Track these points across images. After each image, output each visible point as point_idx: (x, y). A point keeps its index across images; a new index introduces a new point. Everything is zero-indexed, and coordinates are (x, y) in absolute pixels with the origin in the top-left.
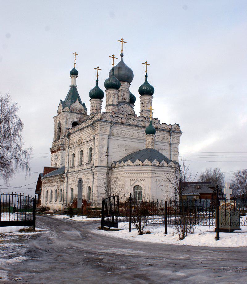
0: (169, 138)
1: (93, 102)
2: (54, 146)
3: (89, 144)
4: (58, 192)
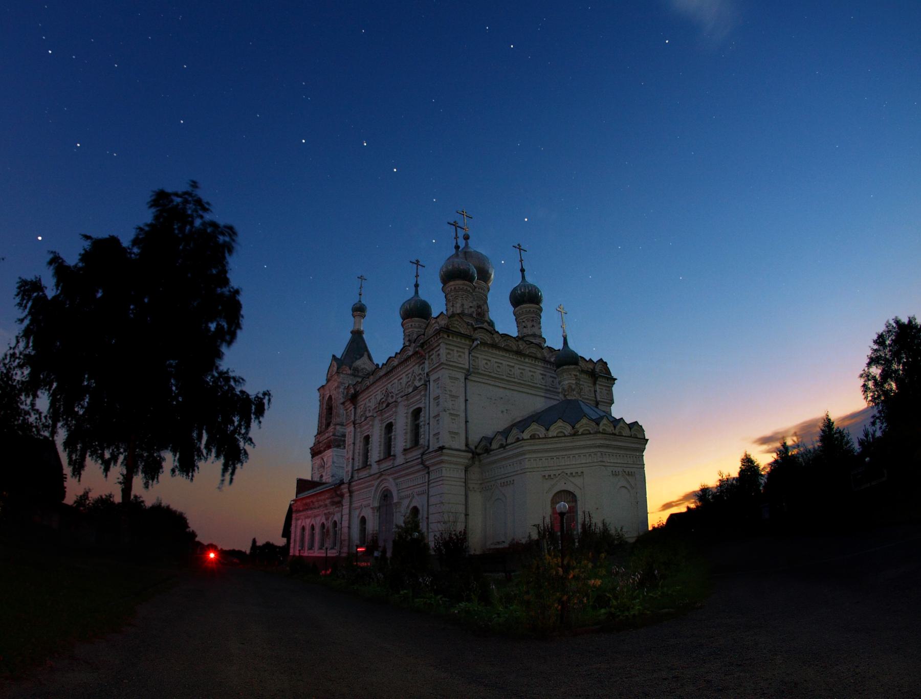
0: (592, 389)
1: (410, 324)
2: (319, 442)
3: (411, 401)
4: (326, 528)
